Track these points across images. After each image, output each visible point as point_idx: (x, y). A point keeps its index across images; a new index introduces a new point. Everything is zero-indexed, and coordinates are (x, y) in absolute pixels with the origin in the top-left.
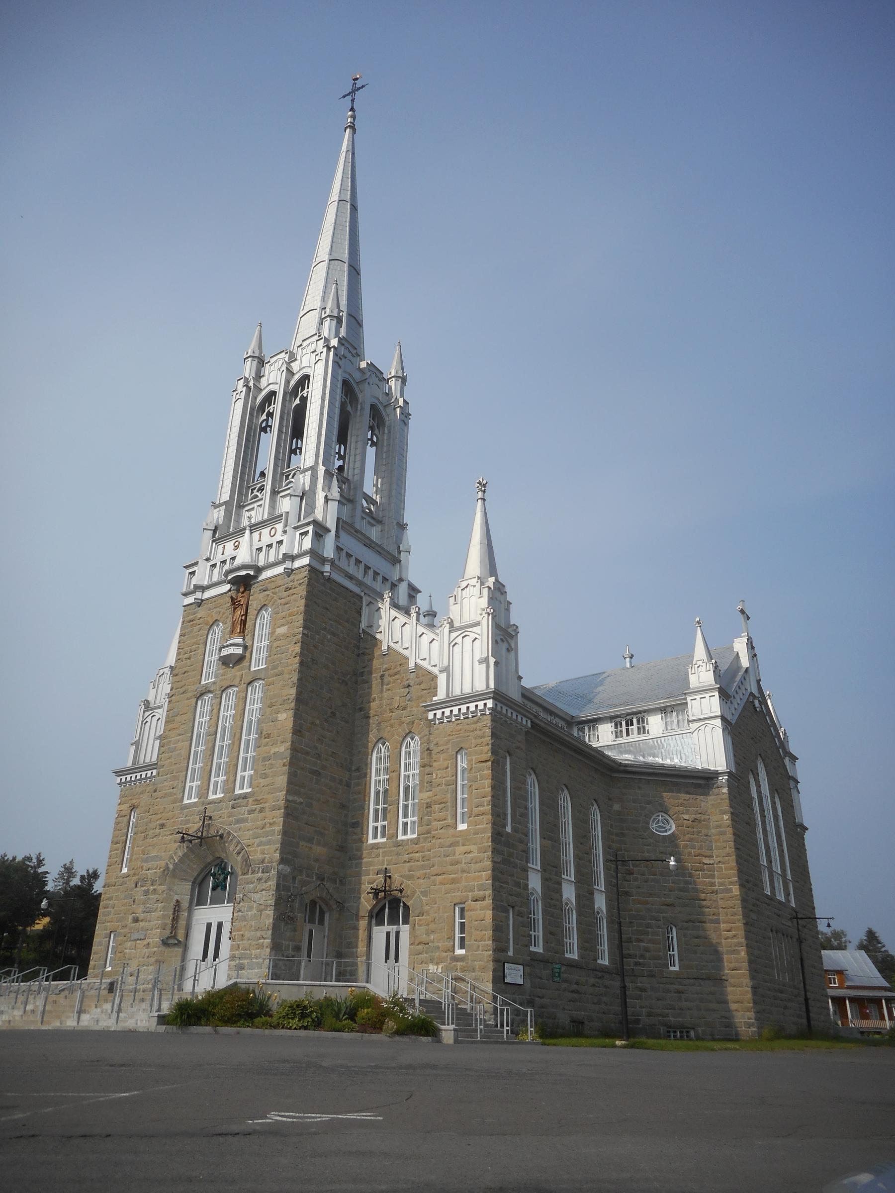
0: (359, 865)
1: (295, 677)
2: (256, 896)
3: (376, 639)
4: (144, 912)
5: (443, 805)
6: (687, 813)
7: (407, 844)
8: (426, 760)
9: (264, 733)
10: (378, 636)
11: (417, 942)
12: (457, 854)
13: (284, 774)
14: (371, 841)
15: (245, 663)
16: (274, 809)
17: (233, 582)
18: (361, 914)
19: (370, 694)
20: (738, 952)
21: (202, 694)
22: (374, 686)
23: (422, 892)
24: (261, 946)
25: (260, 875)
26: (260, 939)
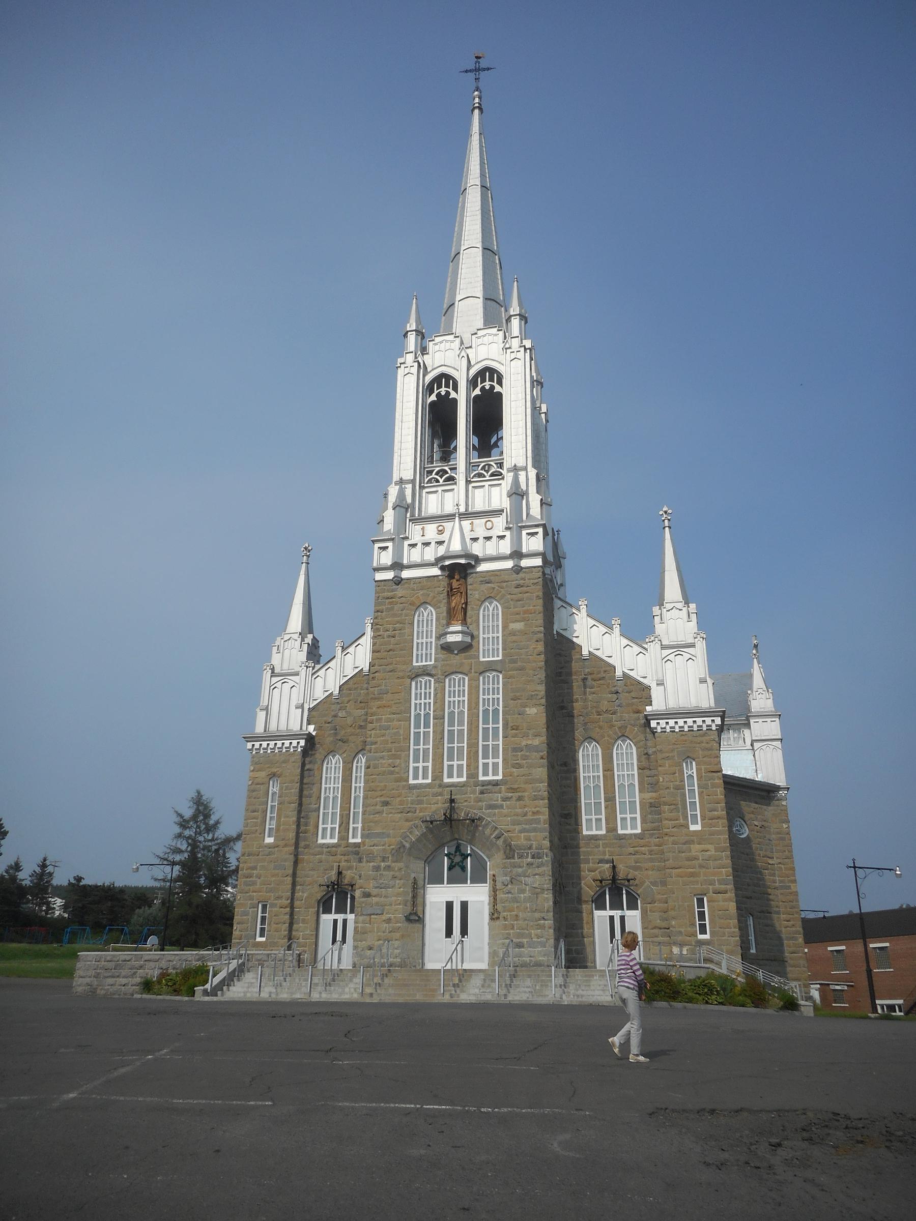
0: (578, 854)
1: (542, 675)
2: (529, 880)
3: (573, 642)
4: (376, 887)
5: (673, 807)
6: (756, 819)
7: (631, 838)
8: (645, 763)
9: (510, 724)
10: (575, 640)
11: (650, 927)
12: (693, 851)
13: (543, 766)
14: (585, 832)
15: (472, 652)
16: (535, 798)
17: (442, 568)
18: (584, 898)
19: (571, 694)
20: (796, 939)
21: (417, 676)
22: (575, 687)
23: (651, 883)
24: (542, 927)
25: (529, 860)
26: (540, 920)
